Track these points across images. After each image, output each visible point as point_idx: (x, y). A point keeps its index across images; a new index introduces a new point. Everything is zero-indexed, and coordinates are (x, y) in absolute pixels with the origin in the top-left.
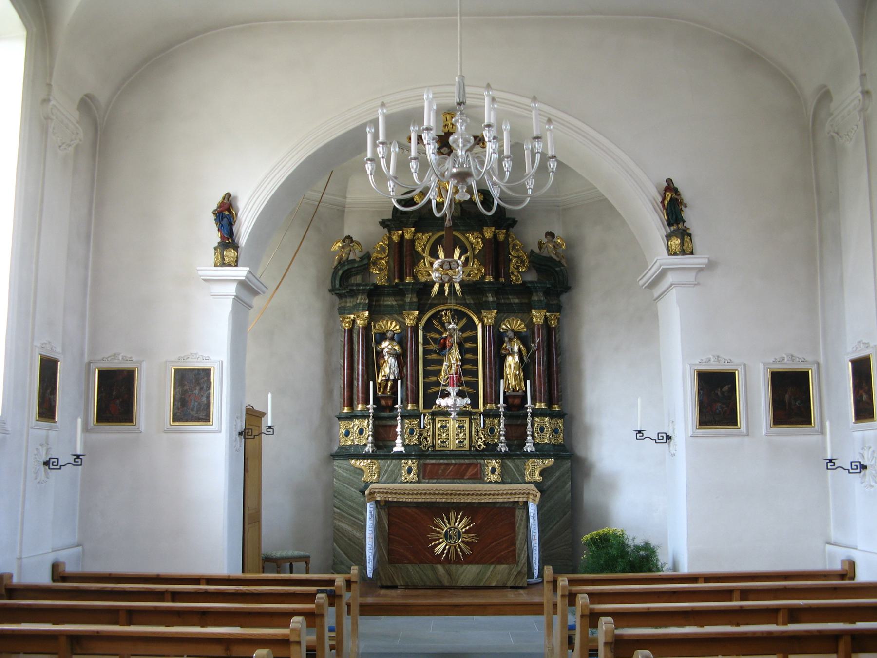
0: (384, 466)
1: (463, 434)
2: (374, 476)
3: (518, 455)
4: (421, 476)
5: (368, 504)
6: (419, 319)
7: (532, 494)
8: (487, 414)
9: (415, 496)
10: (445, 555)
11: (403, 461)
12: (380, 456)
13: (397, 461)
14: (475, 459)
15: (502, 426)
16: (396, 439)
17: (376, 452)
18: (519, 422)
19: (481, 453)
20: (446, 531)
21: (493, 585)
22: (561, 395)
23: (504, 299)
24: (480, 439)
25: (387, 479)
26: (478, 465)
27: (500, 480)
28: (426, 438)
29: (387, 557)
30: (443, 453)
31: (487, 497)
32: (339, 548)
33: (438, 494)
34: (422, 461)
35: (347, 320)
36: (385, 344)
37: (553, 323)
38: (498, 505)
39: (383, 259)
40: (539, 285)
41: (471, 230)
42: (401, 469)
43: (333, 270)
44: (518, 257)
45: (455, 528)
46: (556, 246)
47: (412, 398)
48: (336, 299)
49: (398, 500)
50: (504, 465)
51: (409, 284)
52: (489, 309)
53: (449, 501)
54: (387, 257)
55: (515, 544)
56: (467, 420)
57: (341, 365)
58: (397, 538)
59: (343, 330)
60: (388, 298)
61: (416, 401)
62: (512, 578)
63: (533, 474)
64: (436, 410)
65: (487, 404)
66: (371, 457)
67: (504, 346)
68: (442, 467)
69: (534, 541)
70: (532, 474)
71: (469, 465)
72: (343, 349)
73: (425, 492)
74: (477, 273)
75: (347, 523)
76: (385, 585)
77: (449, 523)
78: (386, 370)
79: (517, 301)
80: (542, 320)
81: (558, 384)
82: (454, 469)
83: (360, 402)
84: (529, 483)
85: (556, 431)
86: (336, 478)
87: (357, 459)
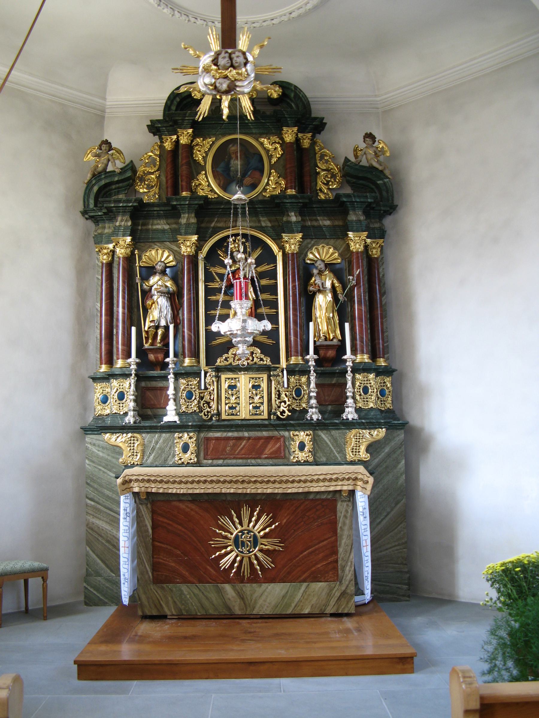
0: (151, 442)
1: (258, 397)
2: (136, 455)
3: (335, 425)
4: (202, 455)
5: (122, 498)
6: (199, 247)
7: (362, 480)
8: (292, 371)
9: (190, 486)
10: (235, 570)
11: (176, 435)
12: (145, 428)
13: (168, 435)
14: (277, 430)
15: (313, 385)
16: (167, 405)
17: (140, 423)
18: (334, 381)
19: (284, 422)
20: (237, 536)
21: (306, 611)
22: (387, 346)
23: (311, 220)
24: (283, 404)
25: (155, 459)
26: (279, 439)
27: (311, 459)
28: (208, 403)
29: (150, 574)
30: (232, 423)
31: (296, 484)
32: (93, 552)
33: (224, 482)
34: (202, 435)
35: (105, 251)
36: (154, 280)
37: (375, 253)
38: (311, 497)
39: (152, 173)
40: (358, 200)
41: (267, 134)
42: (173, 445)
43: (85, 185)
44: (327, 170)
45: (249, 531)
46: (377, 152)
47: (190, 350)
48: (90, 224)
49: (166, 491)
50: (317, 438)
51: (185, 198)
52: (292, 231)
53: (240, 491)
54: (157, 171)
55: (336, 552)
56: (265, 376)
57: (97, 309)
58: (165, 546)
59: (100, 264)
60: (159, 221)
61: (195, 354)
62: (332, 602)
63: (358, 451)
64: (222, 364)
65: (291, 356)
66: (131, 429)
67: (312, 281)
68: (231, 443)
69: (365, 548)
70: (355, 450)
71: (269, 439)
72: (100, 289)
73: (204, 478)
74: (275, 188)
75: (105, 519)
76: (148, 613)
77: (241, 524)
78: (154, 314)
79: (328, 223)
80: (362, 246)
81: (383, 332)
82: (247, 445)
83: (120, 356)
84: (352, 463)
85: (382, 393)
86: (89, 459)
87: (113, 433)
